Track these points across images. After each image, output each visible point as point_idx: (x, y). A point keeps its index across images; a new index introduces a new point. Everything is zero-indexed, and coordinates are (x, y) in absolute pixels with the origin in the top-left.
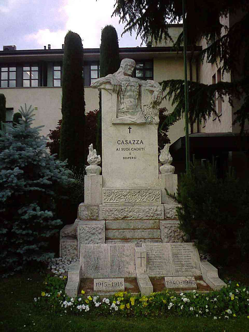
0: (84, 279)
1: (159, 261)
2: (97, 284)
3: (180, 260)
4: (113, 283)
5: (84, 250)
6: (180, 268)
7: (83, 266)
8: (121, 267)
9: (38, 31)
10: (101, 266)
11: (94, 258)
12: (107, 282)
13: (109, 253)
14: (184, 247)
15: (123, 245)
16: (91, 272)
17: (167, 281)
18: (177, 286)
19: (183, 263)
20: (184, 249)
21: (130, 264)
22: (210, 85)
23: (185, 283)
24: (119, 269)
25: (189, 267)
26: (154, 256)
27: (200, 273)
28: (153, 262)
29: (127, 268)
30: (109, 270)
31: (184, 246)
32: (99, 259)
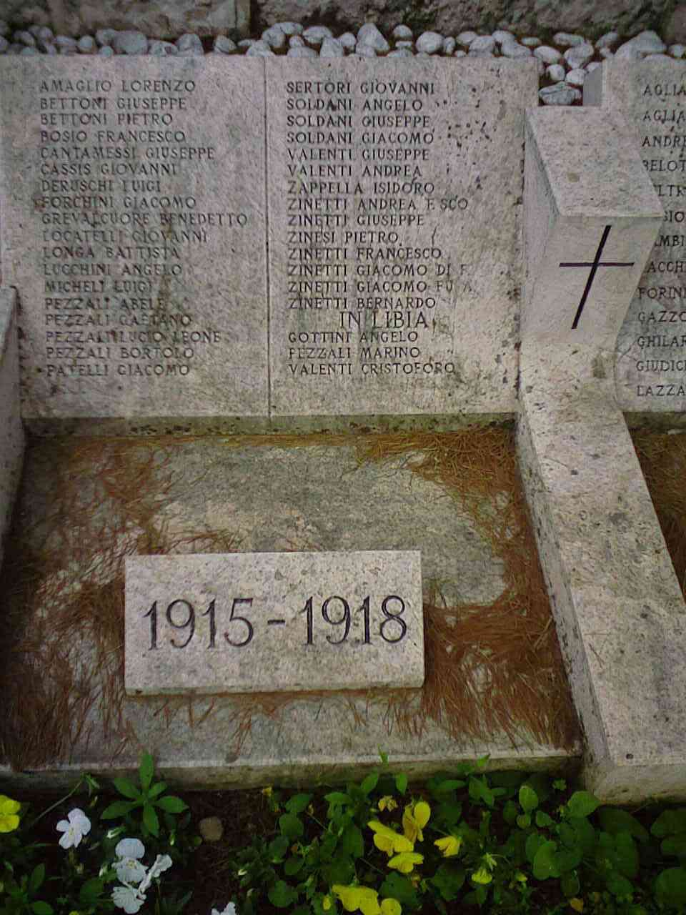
0: (51, 423)
2: (161, 618)
4: (317, 610)
5: (37, 121)
7: (35, 300)
8: (381, 320)
9: (651, 798)
10: (201, 302)
11: (138, 217)
12: (258, 589)
13: (279, 166)
15: (418, 78)
16: (116, 353)
21: (468, 287)
24: (371, 334)
29: (441, 326)
30: (279, 345)
32: (180, 228)
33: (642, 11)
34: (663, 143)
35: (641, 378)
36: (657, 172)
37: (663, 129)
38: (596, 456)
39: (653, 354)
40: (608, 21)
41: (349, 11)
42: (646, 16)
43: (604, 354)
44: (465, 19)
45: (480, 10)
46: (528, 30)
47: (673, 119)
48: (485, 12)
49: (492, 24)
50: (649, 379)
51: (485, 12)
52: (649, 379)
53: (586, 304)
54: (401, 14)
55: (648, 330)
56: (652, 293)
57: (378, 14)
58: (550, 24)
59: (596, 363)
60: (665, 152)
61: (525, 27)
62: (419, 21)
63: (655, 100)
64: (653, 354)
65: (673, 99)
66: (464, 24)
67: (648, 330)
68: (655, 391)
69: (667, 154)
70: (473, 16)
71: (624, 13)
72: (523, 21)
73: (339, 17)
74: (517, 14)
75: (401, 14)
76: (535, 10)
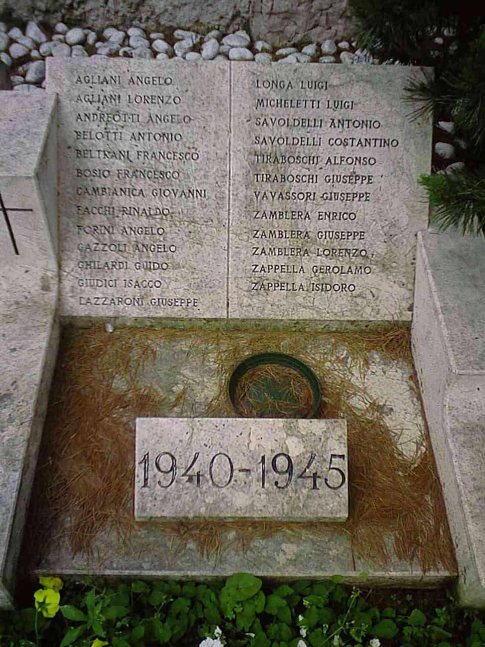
1: (156, 203)
3: (290, 205)
4: (152, 462)
6: (283, 261)
14: (338, 104)
17: (145, 460)
18: (209, 500)
19: (311, 226)
20: (338, 115)
22: (34, 594)
23: (272, 475)
25: (342, 262)
26: (121, 164)
27: (405, 305)
28: (110, 211)
31: (347, 95)
33: (234, 17)
34: (92, 119)
35: (82, 291)
36: (88, 141)
37: (92, 109)
38: (14, 350)
39: (90, 274)
40: (213, 23)
41: (21, 12)
42: (238, 20)
43: (49, 274)
44: (108, 19)
45: (116, 13)
46: (155, 27)
47: (99, 101)
48: (120, 14)
49: (128, 22)
50: (88, 292)
51: (120, 14)
52: (88, 292)
53: (16, 237)
54: (59, 15)
55: (86, 257)
56: (87, 230)
57: (43, 15)
58: (171, 24)
59: (44, 279)
60: (94, 126)
61: (153, 26)
62: (74, 20)
63: (84, 86)
64: (90, 274)
65: (99, 86)
66: (107, 23)
67: (86, 257)
68: (93, 301)
69: (95, 127)
70: (112, 17)
71: (222, 18)
72: (150, 21)
73: (14, 15)
74: (144, 17)
75: (59, 15)
76: (157, 14)
